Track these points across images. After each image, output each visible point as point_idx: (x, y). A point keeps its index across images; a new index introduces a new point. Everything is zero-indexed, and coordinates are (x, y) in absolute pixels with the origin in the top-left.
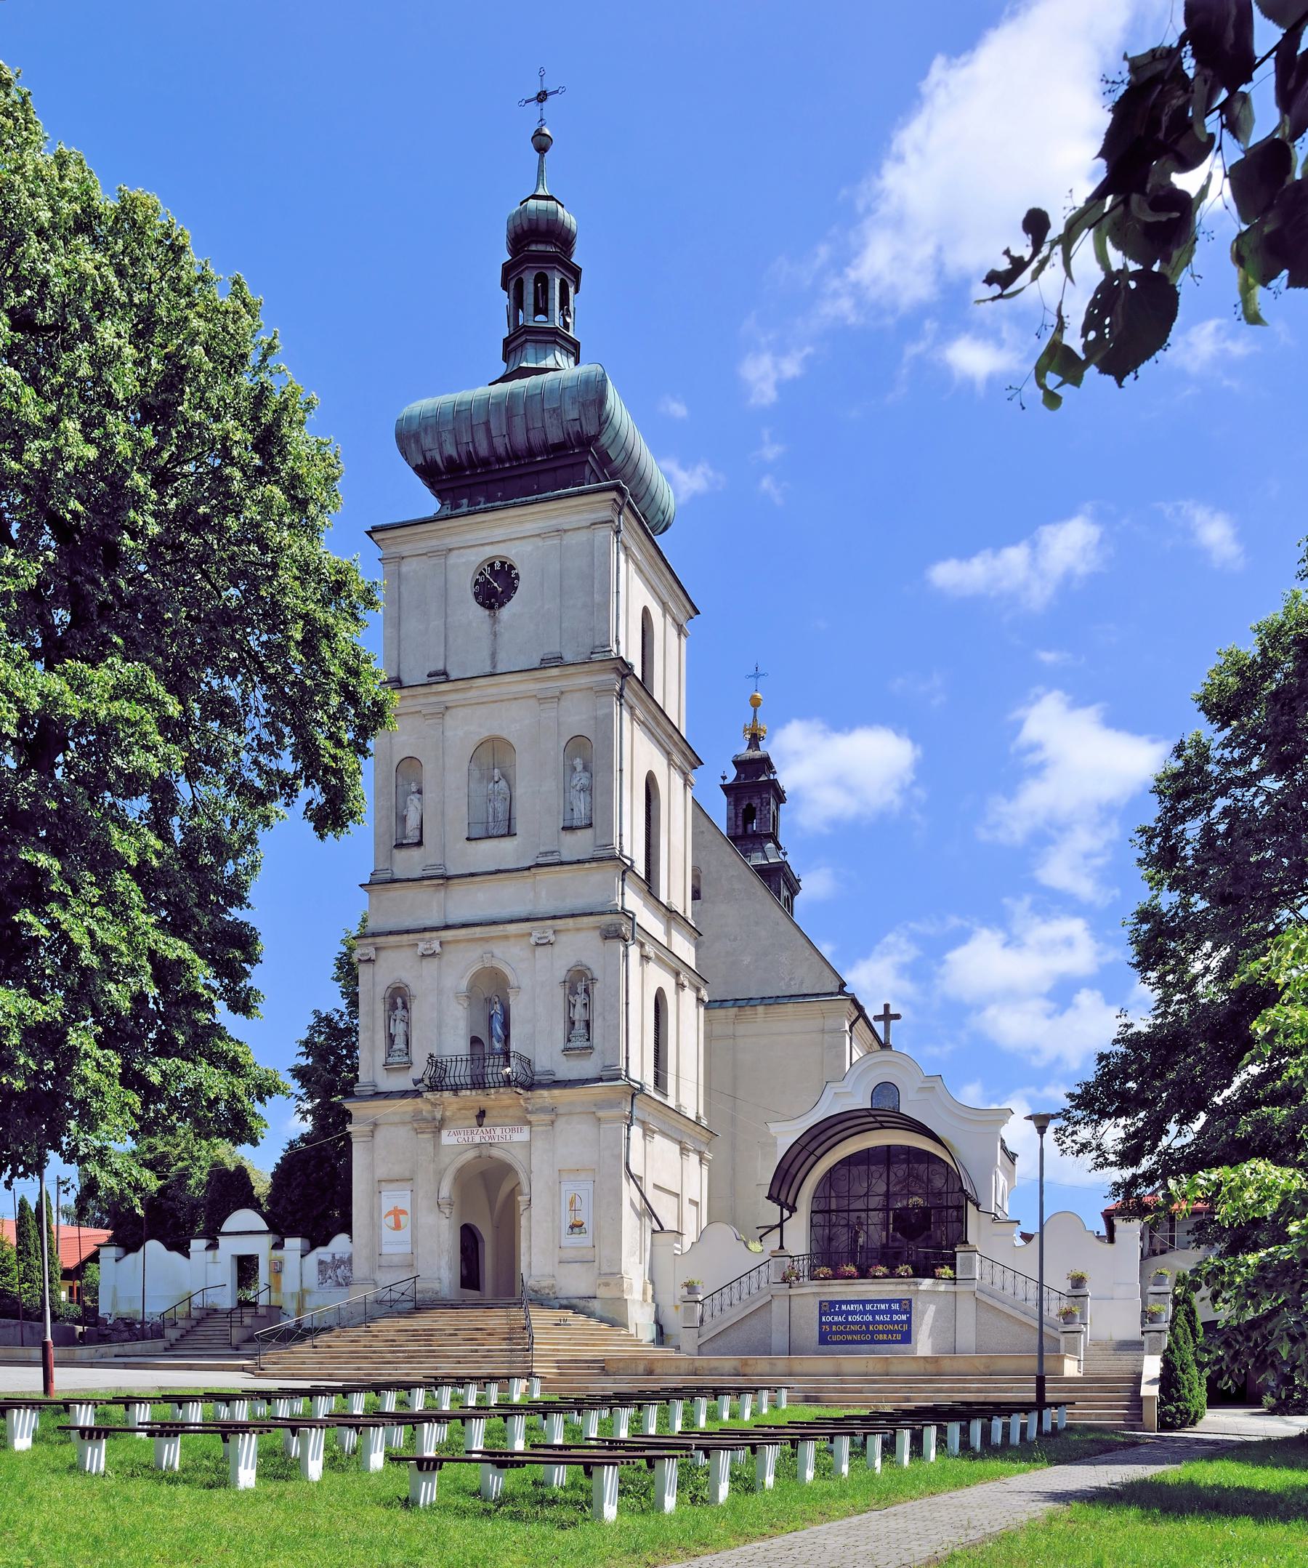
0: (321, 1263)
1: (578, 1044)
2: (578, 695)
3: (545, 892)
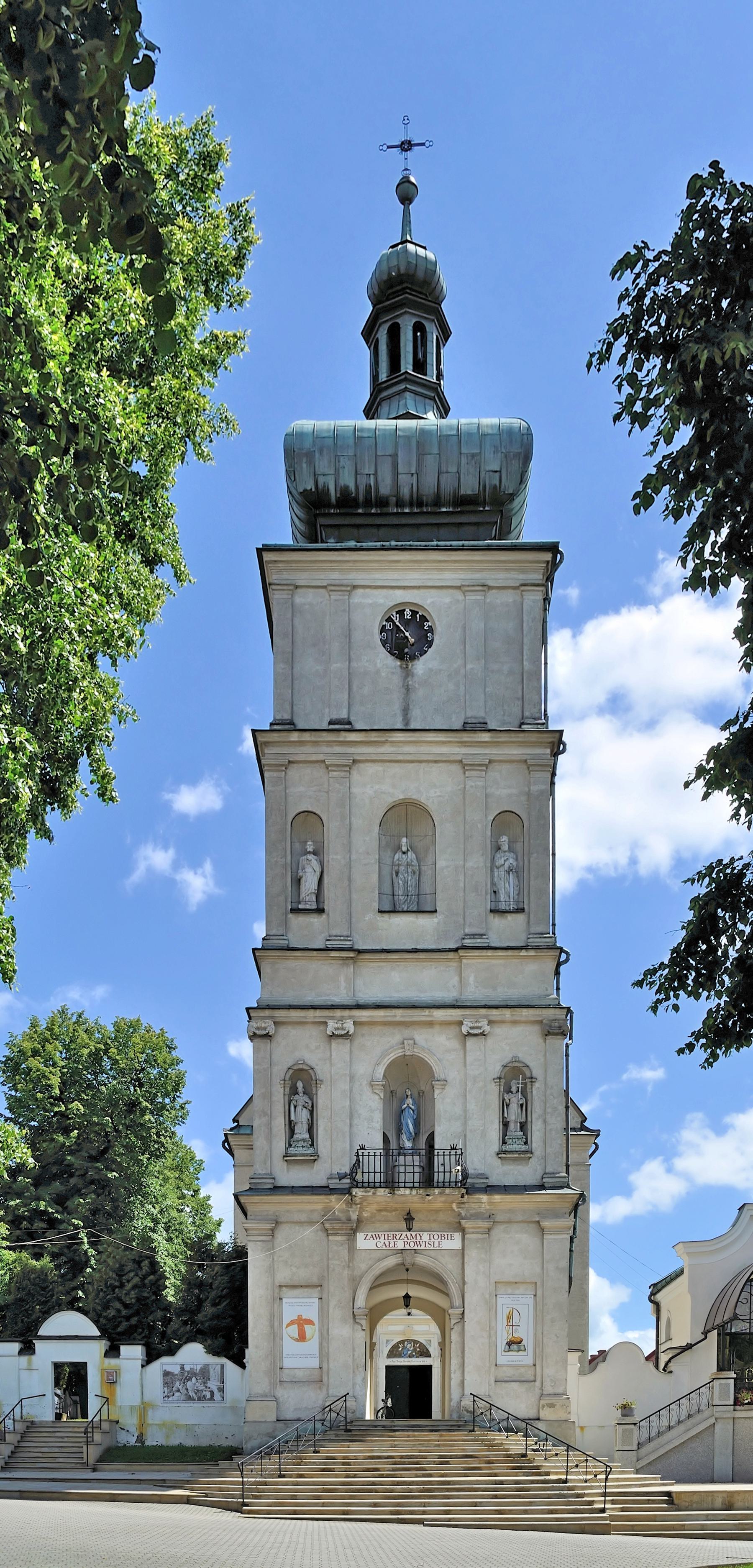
0: (166, 1374)
1: (515, 1147)
2: (505, 767)
3: (475, 978)
